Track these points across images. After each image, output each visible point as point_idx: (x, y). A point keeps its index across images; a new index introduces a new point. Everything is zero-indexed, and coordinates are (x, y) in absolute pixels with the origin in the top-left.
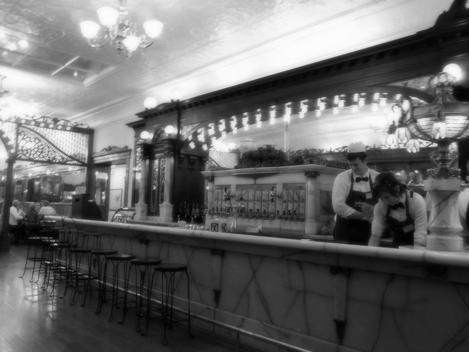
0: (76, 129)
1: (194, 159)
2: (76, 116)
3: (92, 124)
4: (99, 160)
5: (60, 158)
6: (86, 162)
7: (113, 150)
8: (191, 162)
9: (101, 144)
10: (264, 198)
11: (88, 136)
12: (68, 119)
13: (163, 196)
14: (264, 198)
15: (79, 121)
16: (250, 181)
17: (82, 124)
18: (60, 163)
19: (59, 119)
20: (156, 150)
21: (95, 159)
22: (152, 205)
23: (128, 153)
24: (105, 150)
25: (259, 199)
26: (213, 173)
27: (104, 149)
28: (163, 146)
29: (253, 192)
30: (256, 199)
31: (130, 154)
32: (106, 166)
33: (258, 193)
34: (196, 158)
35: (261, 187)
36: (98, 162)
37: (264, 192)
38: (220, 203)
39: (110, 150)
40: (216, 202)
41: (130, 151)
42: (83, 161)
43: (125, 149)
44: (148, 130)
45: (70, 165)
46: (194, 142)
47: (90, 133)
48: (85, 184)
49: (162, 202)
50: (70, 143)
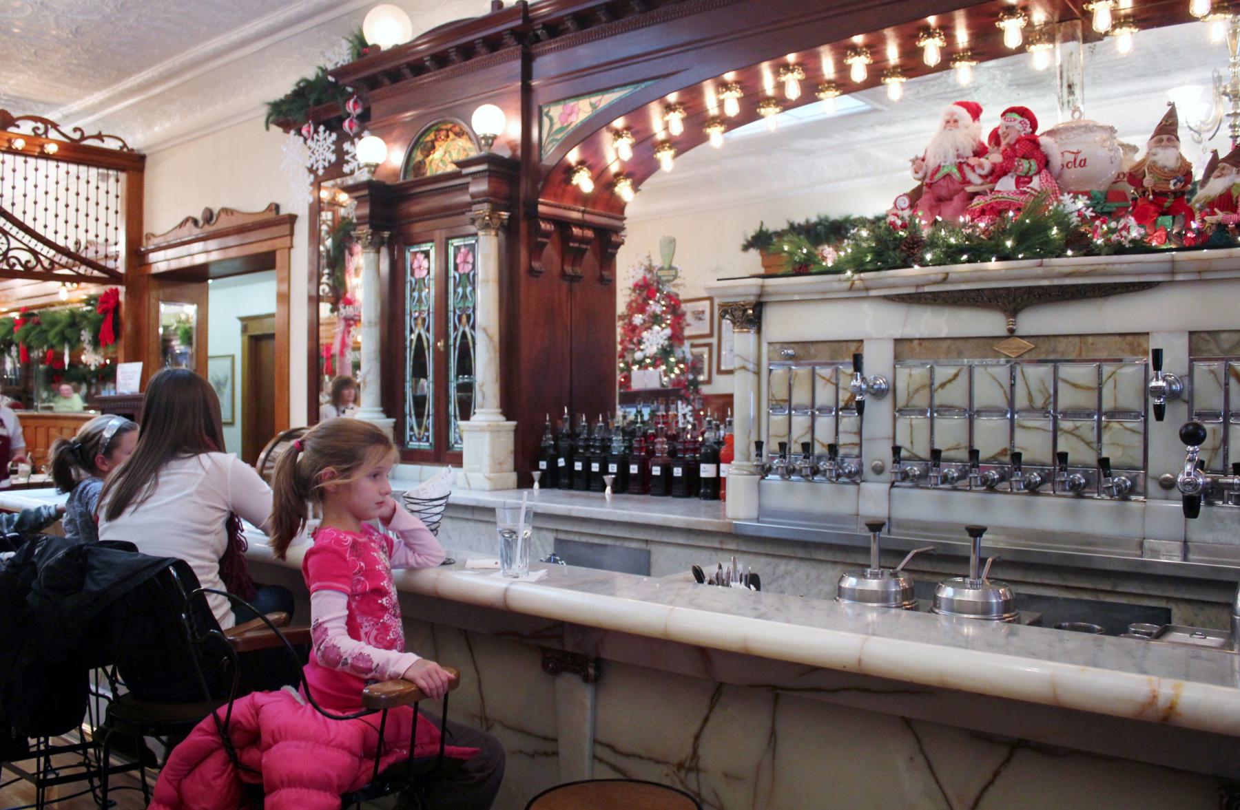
0: (78, 153)
1: (582, 240)
2: (76, 106)
3: (136, 140)
4: (161, 262)
5: (25, 256)
6: (121, 267)
7: (223, 223)
8: (571, 253)
9: (167, 210)
10: (1067, 398)
11: (123, 176)
12: (51, 116)
13: (467, 389)
14: (1067, 398)
15: (89, 125)
16: (989, 323)
17: (100, 137)
18: (28, 273)
19: (15, 114)
20: (416, 208)
21: (152, 257)
22: (411, 420)
23: (285, 229)
24: (190, 224)
25: (1039, 401)
26: (762, 286)
27: (187, 220)
28: (465, 187)
29: (1002, 372)
30: (1021, 401)
31: (292, 234)
32: (191, 280)
33: (1036, 374)
34: (589, 234)
35: (1047, 350)
36: (161, 267)
37: (1066, 371)
38: (800, 422)
39: (209, 224)
40: (779, 418)
41: (292, 219)
42: (110, 264)
43: (272, 215)
44: (383, 132)
45: (63, 279)
46: (590, 168)
47: (131, 164)
48: (199, 374)
49: (466, 414)
50: (62, 203)
